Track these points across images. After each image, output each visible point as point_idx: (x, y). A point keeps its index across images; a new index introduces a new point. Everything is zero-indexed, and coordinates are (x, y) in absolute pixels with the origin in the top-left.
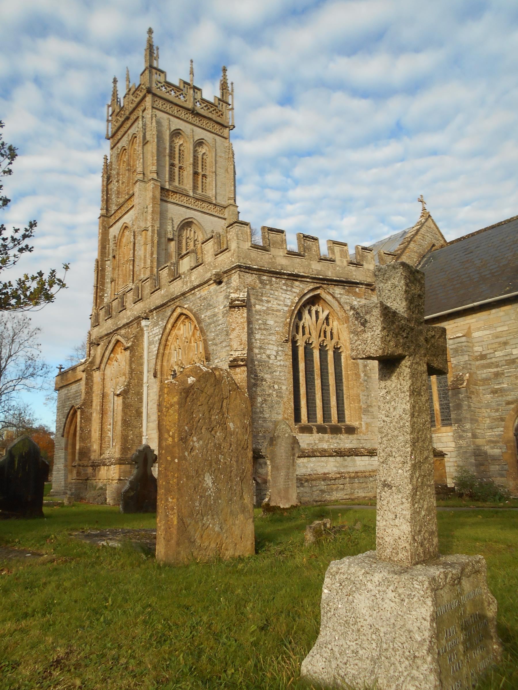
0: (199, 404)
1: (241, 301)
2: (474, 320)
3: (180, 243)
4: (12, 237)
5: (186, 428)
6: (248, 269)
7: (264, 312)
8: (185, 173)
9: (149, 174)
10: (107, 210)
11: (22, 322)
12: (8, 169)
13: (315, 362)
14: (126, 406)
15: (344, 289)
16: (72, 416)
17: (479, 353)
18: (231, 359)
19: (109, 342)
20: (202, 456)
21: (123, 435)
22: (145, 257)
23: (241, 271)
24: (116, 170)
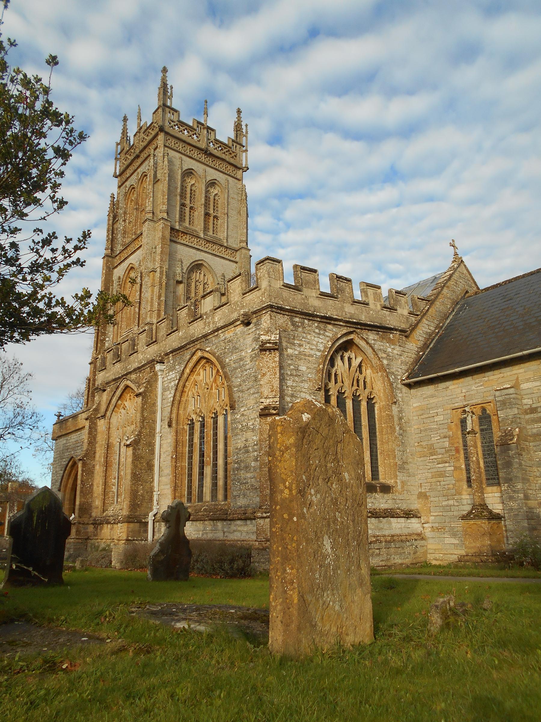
0: (315, 448)
1: (273, 343)
2: (522, 371)
3: (189, 285)
4: (64, 247)
5: (304, 477)
6: (280, 310)
7: (296, 356)
8: (196, 213)
9: (159, 213)
10: (112, 250)
11: (12, 367)
12: (60, 170)
13: (347, 413)
14: (136, 458)
15: (378, 334)
16: (72, 469)
17: (529, 406)
18: (262, 407)
19: (118, 388)
20: (320, 513)
21: (132, 490)
22: (152, 299)
23: (273, 312)
24: (124, 209)
